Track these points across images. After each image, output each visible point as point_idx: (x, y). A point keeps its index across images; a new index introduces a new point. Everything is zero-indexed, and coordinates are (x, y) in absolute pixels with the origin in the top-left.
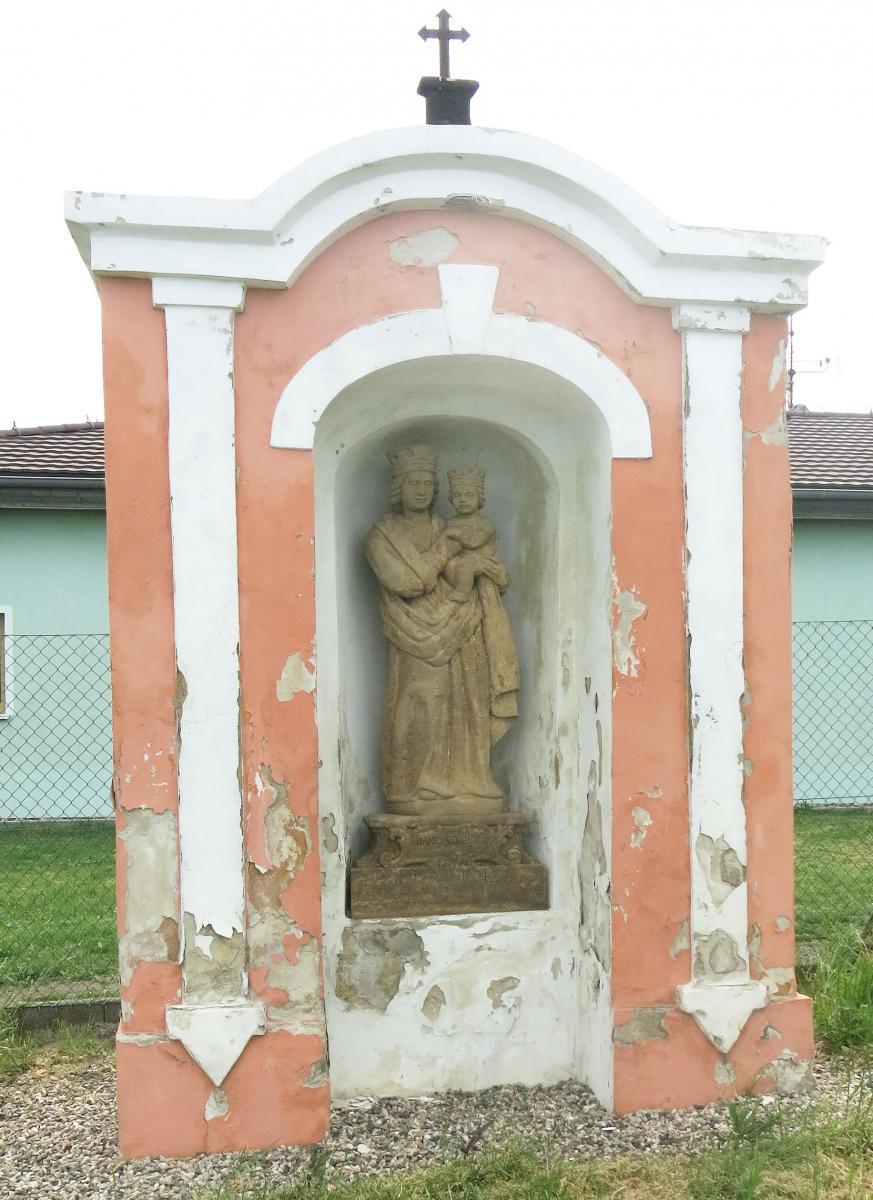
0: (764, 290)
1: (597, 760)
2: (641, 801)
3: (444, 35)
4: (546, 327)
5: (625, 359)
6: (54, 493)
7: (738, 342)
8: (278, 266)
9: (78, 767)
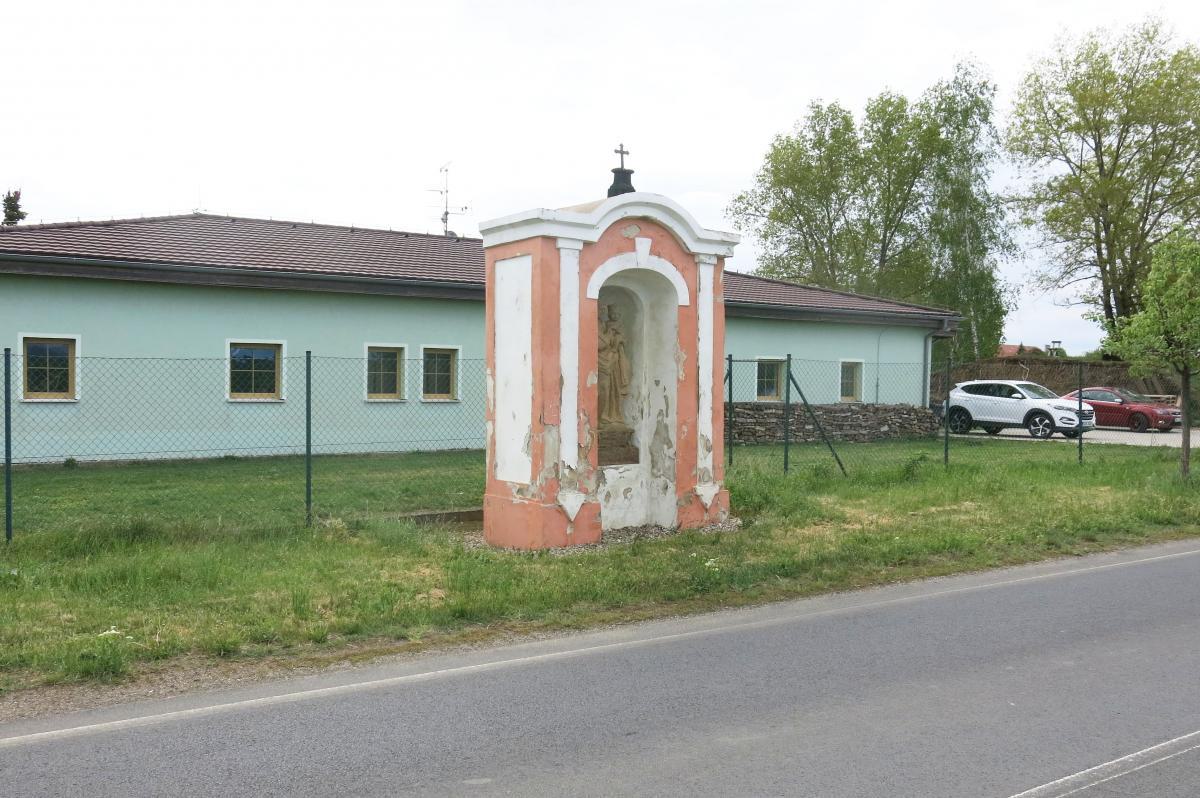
0: (722, 251)
1: (664, 409)
2: (685, 423)
3: (622, 153)
4: (663, 260)
5: (682, 271)
6: (118, 270)
7: (712, 267)
8: (594, 236)
9: (213, 430)
